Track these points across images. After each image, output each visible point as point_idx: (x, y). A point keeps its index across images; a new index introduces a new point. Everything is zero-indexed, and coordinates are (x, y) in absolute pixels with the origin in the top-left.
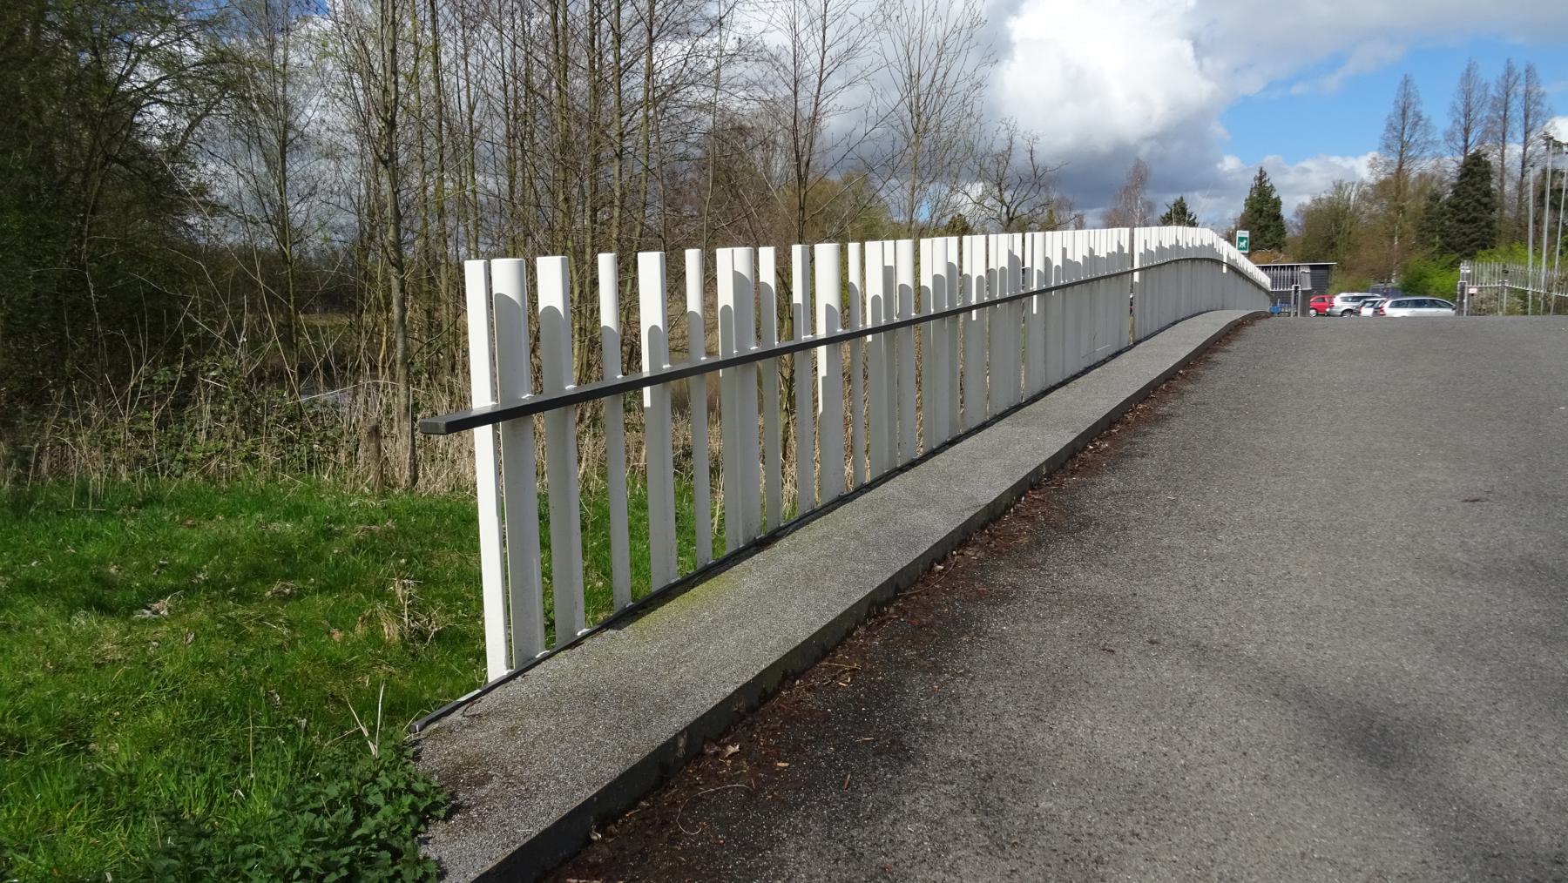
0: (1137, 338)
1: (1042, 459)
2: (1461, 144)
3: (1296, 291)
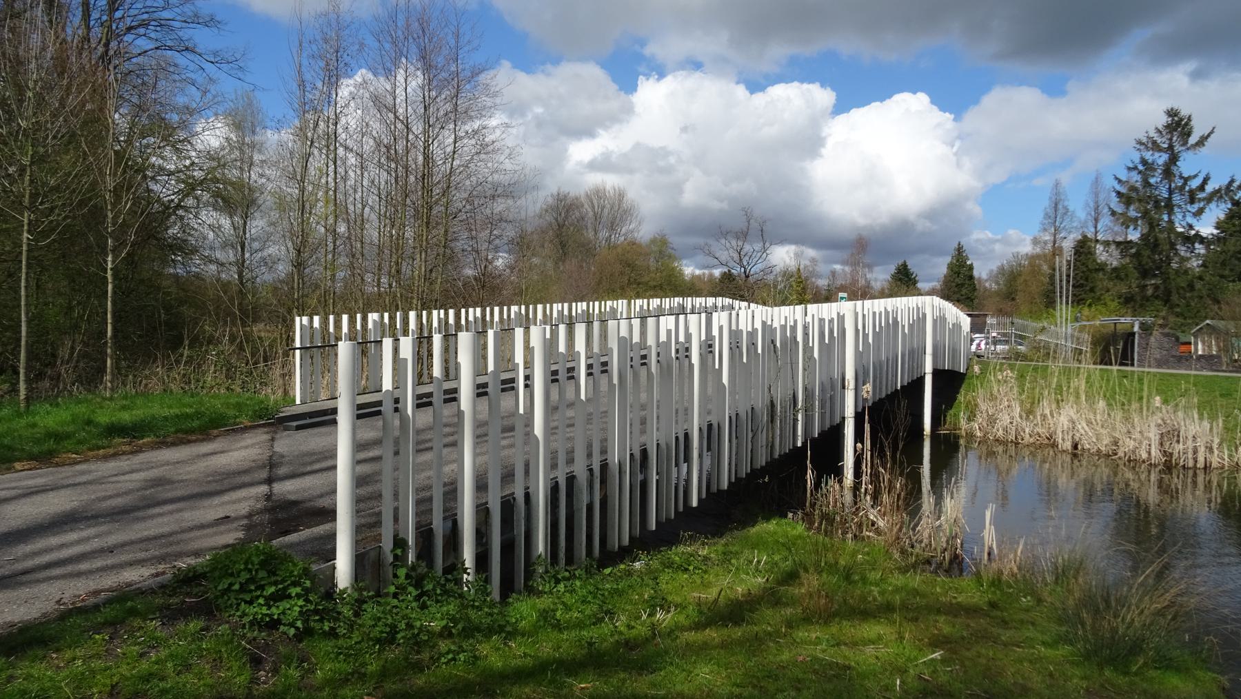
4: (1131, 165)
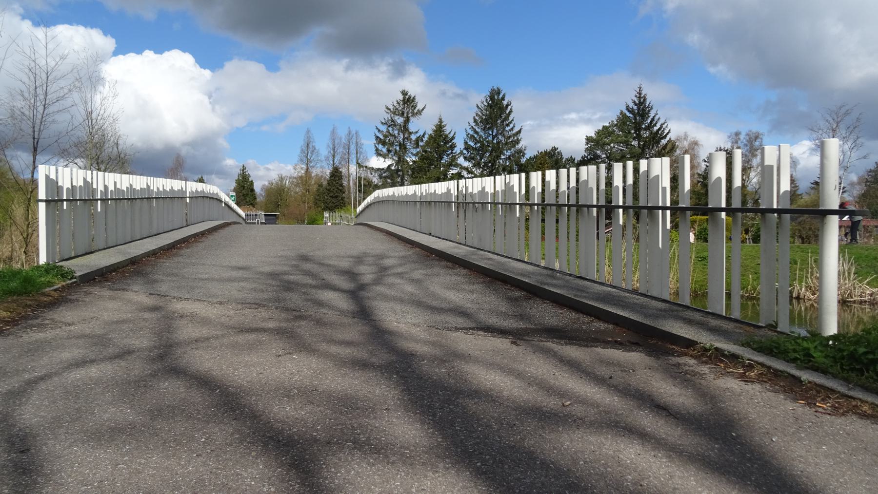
2: (332, 162)
4: (384, 121)
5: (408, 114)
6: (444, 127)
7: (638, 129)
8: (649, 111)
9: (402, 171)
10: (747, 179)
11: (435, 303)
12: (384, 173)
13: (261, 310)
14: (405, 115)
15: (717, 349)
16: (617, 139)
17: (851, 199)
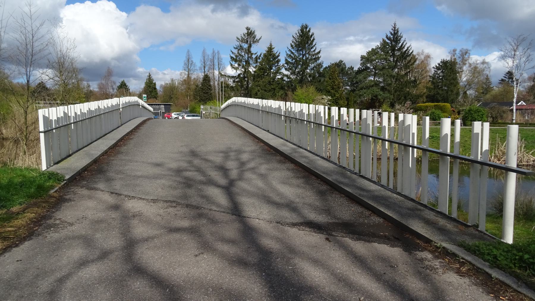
0: (122, 123)
1: (112, 144)
2: (203, 71)
3: (161, 112)
4: (235, 47)
5: (250, 42)
6: (273, 49)
7: (393, 50)
8: (400, 39)
9: (248, 78)
10: (460, 79)
11: (277, 199)
12: (237, 79)
13: (178, 208)
14: (249, 43)
15: (444, 248)
16: (380, 57)
17: (524, 89)
